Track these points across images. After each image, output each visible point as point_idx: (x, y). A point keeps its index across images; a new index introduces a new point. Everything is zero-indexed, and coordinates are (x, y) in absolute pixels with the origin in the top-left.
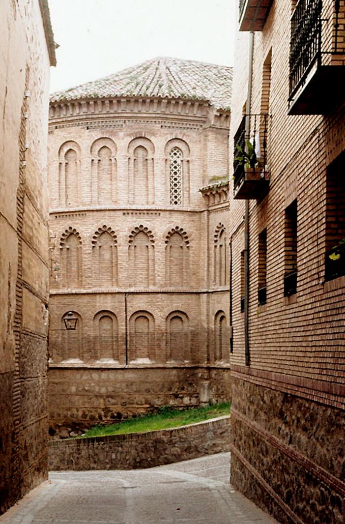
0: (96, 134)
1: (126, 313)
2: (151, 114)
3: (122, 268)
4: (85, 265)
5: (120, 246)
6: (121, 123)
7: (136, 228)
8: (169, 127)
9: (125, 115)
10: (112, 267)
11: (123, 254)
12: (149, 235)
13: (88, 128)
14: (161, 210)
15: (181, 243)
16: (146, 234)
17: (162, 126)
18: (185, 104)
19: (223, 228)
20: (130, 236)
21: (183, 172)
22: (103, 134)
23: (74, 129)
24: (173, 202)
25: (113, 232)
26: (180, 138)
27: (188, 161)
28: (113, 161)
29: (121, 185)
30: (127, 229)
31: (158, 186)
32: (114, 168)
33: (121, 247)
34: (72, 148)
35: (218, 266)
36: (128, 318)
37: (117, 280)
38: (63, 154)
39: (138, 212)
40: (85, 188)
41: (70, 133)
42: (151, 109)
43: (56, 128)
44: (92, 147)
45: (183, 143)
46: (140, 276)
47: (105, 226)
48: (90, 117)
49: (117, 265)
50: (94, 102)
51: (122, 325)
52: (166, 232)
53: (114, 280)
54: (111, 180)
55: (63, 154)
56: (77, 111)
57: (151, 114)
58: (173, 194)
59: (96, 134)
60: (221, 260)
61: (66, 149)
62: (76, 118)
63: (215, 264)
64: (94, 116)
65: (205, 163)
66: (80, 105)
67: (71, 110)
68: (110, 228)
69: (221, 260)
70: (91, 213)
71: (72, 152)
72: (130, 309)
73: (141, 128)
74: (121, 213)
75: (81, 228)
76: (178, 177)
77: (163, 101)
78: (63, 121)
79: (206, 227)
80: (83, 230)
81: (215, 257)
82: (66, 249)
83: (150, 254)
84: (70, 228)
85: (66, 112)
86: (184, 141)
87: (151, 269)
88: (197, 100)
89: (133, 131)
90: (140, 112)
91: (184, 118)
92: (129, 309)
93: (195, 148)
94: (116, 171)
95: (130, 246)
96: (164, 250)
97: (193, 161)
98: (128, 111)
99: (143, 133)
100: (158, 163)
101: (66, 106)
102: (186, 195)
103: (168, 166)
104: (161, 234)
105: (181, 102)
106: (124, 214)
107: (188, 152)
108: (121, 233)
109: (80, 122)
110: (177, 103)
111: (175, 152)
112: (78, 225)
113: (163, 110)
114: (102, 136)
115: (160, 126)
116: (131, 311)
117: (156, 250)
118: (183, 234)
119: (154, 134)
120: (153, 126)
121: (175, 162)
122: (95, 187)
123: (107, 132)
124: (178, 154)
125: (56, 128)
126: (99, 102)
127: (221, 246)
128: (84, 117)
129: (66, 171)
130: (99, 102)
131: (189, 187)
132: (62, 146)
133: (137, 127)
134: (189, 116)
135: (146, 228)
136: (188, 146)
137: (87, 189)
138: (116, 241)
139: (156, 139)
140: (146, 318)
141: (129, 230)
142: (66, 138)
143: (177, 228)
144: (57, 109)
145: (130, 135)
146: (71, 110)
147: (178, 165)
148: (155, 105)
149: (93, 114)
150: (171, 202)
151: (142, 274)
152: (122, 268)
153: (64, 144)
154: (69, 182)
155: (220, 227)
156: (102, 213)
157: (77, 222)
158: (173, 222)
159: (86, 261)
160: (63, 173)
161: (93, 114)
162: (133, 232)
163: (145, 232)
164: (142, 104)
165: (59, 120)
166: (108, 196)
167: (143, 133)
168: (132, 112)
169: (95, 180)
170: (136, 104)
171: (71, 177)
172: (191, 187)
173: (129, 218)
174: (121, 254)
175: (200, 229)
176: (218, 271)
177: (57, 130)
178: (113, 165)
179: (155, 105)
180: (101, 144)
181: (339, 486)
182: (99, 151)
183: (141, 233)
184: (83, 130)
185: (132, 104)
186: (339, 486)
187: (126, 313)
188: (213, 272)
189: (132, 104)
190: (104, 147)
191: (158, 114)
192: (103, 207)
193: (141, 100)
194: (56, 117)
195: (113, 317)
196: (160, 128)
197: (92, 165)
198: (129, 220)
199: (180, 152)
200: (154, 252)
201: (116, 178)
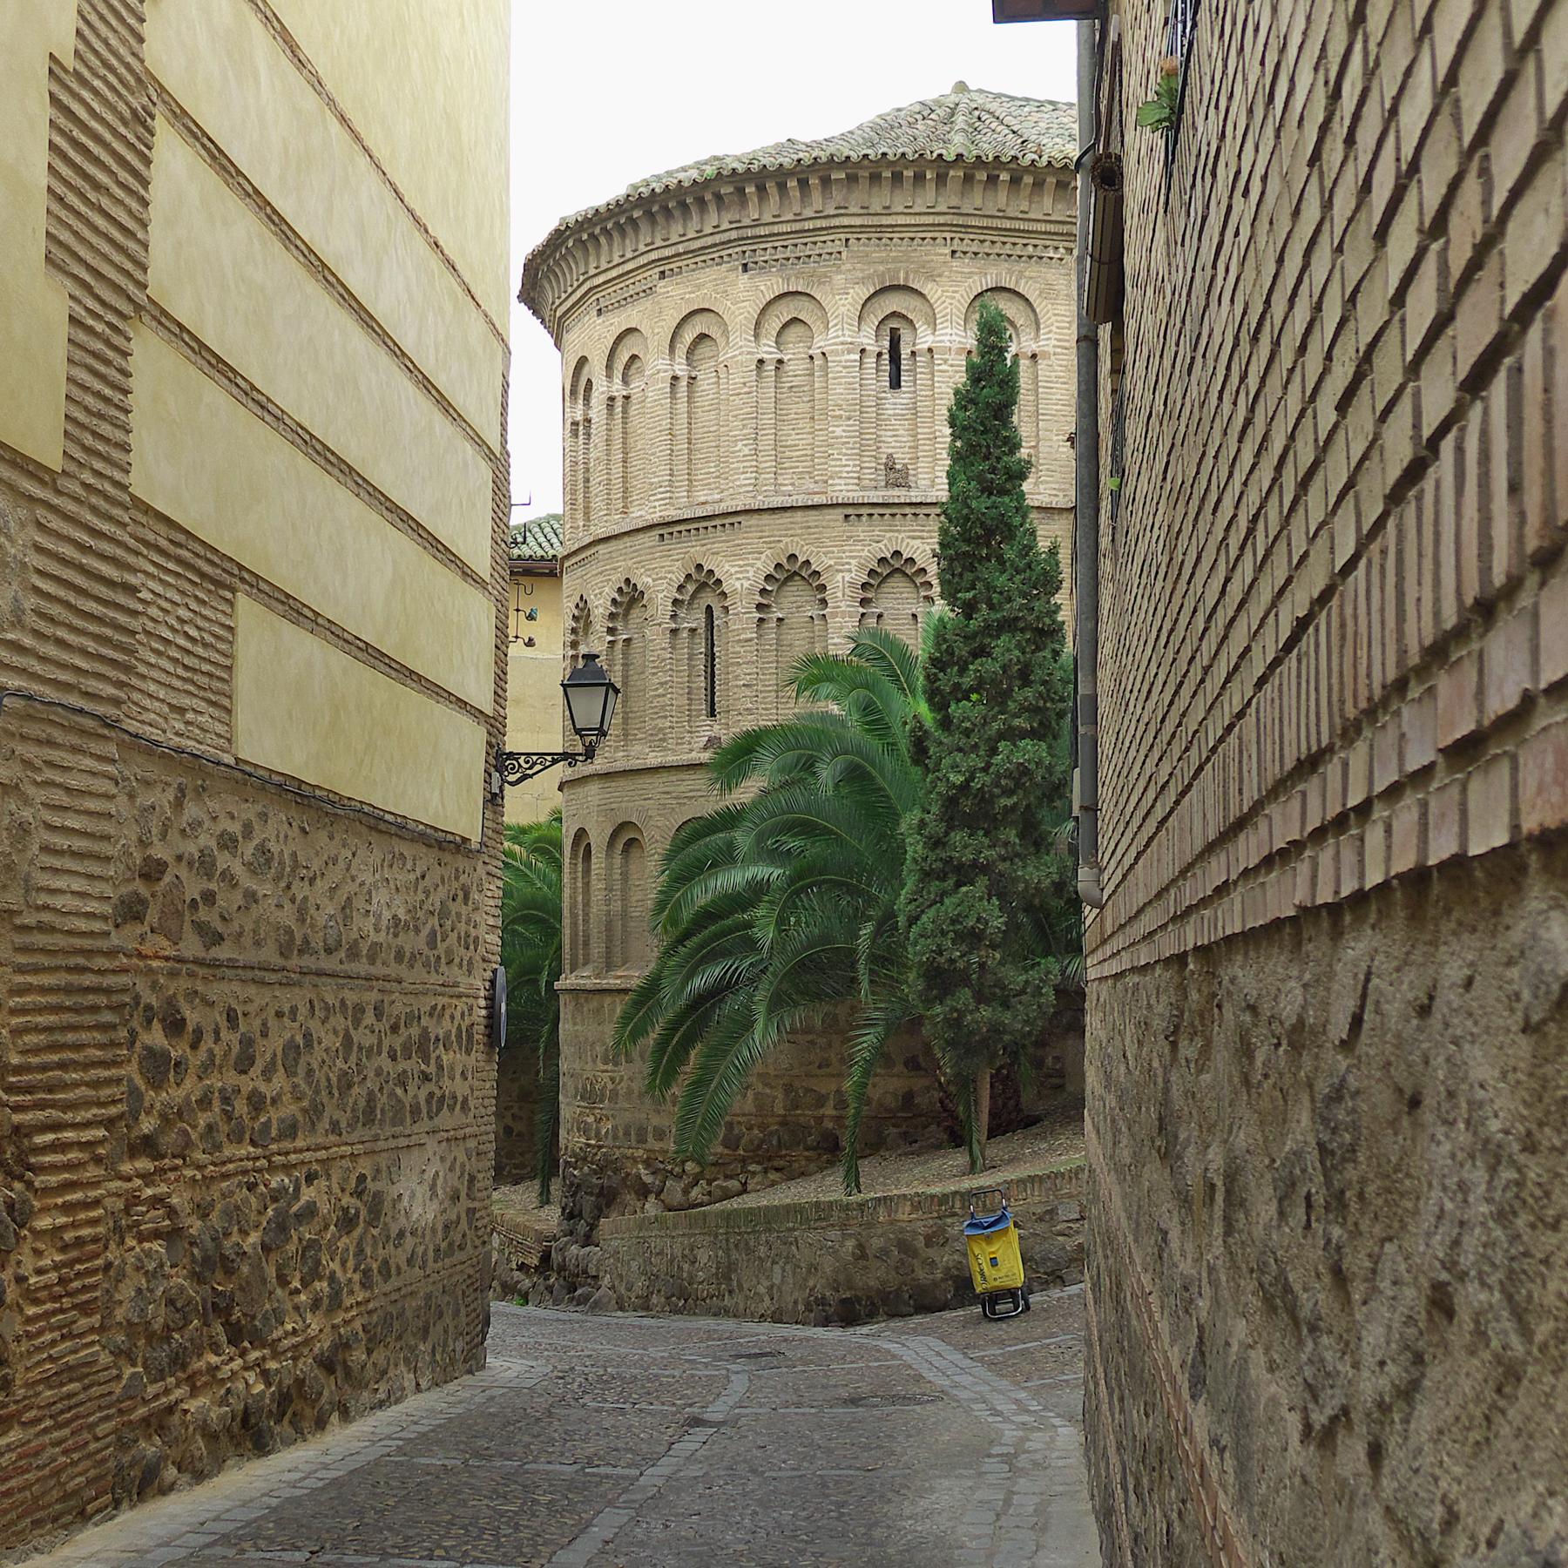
0: (772, 285)
5: (834, 615)
6: (838, 245)
7: (882, 561)
8: (976, 254)
9: (846, 221)
12: (919, 580)
13: (745, 267)
16: (911, 579)
17: (954, 252)
18: (1015, 181)
20: (864, 586)
23: (710, 274)
25: (816, 574)
29: (839, 432)
38: (681, 349)
39: (888, 511)
41: (699, 287)
42: (919, 201)
43: (662, 275)
44: (758, 324)
45: (915, 297)
47: (793, 557)
48: (750, 233)
50: (757, 187)
55: (681, 349)
56: (712, 218)
59: (772, 285)
61: (688, 336)
62: (709, 241)
64: (762, 231)
67: (695, 217)
70: (754, 520)
71: (708, 342)
73: (894, 260)
74: (838, 514)
77: (952, 173)
78: (679, 255)
82: (685, 634)
85: (685, 227)
88: (791, 173)
90: (887, 211)
97: (1046, 355)
98: (852, 210)
99: (902, 275)
101: (683, 206)
105: (1005, 176)
108: (839, 577)
109: (723, 253)
110: (992, 180)
113: (954, 201)
115: (947, 251)
118: (801, 567)
119: (931, 277)
122: (766, 442)
125: (662, 275)
126: (771, 186)
128: (734, 235)
130: (771, 186)
132: (679, 326)
134: (1029, 220)
135: (911, 560)
137: (743, 449)
138: (824, 602)
141: (861, 567)
144: (660, 219)
145: (862, 281)
146: (695, 217)
148: (931, 188)
149: (757, 224)
154: (698, 432)
156: (785, 518)
160: (682, 406)
161: (757, 224)
163: (910, 571)
164: (893, 186)
165: (667, 252)
167: (902, 275)
168: (866, 211)
169: (768, 419)
170: (875, 190)
171: (704, 418)
173: (861, 530)
177: (662, 283)
179: (931, 188)
180: (785, 312)
184: (732, 276)
185: (864, 184)
189: (864, 184)
190: (795, 320)
192: (788, 501)
193: (887, 174)
194: (659, 243)
196: (949, 258)
197: (758, 375)
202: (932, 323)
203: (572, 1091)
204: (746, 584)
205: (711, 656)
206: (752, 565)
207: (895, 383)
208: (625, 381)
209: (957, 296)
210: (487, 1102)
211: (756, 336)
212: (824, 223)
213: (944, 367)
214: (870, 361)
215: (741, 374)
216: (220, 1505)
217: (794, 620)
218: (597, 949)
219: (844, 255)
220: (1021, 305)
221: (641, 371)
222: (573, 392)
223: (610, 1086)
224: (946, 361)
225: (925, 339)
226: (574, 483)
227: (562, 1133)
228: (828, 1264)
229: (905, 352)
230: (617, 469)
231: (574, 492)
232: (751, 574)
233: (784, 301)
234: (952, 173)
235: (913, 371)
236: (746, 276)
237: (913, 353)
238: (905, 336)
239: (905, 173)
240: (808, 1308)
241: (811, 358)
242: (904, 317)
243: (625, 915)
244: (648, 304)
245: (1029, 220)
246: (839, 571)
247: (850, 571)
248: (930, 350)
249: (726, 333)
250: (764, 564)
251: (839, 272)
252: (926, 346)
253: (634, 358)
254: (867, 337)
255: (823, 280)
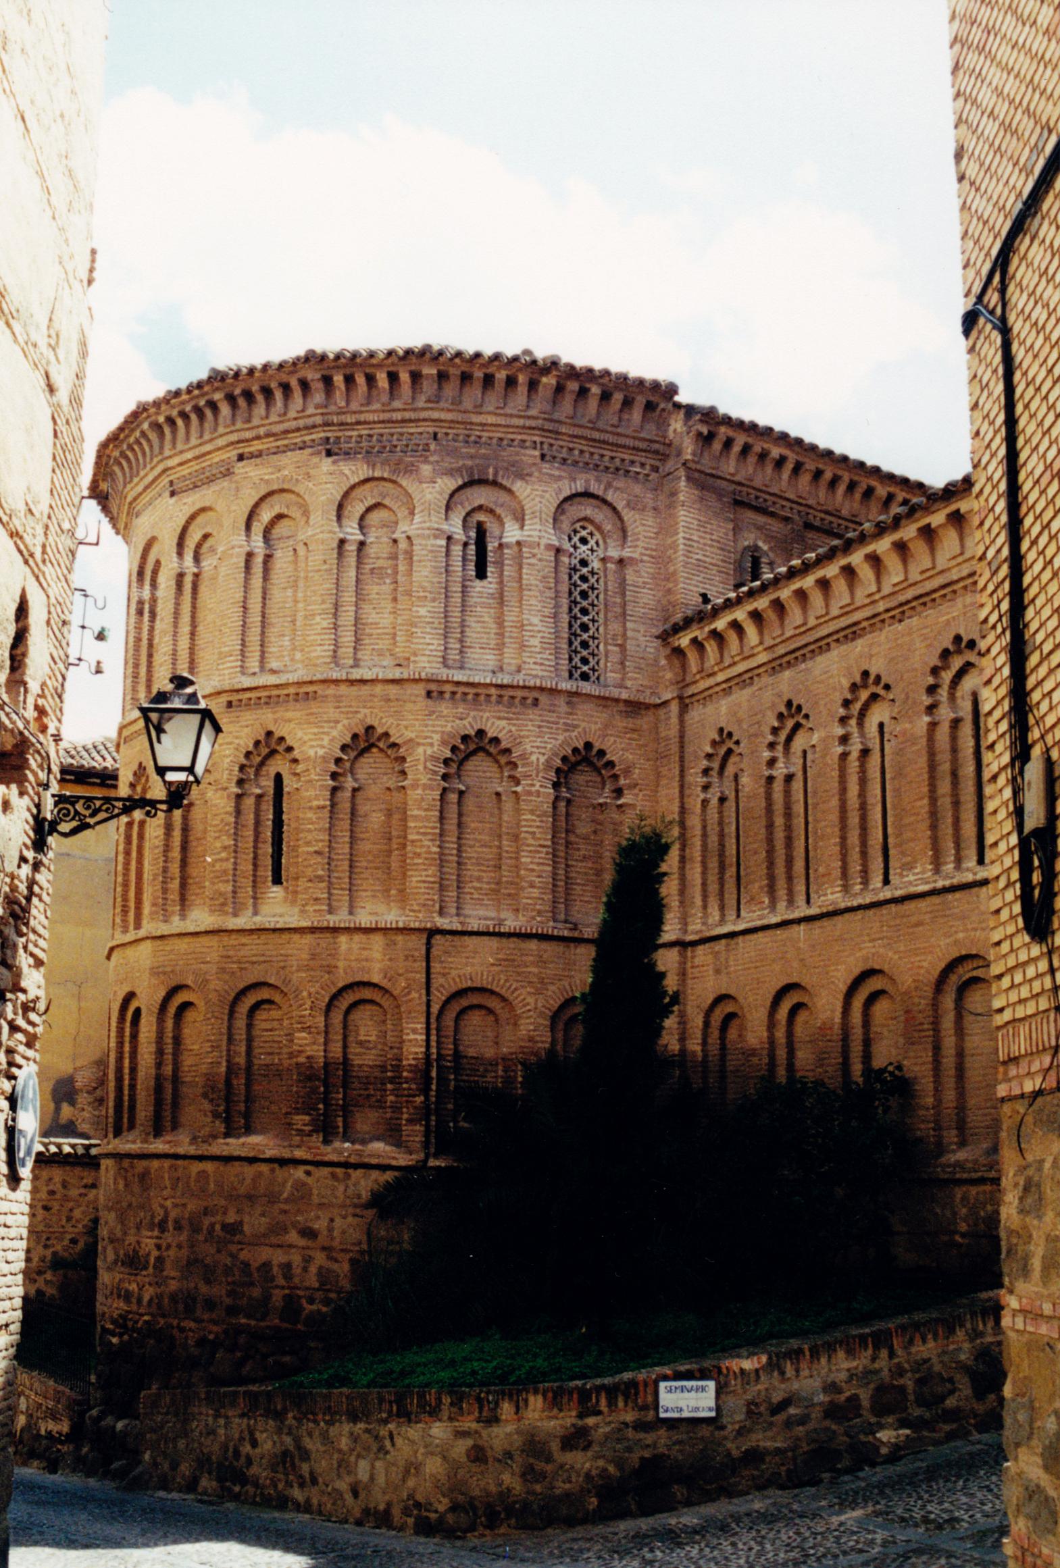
0: (355, 470)
1: (428, 993)
2: (511, 416)
3: (418, 855)
4: (308, 843)
7: (465, 738)
8: (565, 460)
10: (389, 852)
11: (423, 813)
14: (541, 689)
15: (600, 795)
19: (730, 744)
21: (606, 590)
22: (374, 466)
24: (577, 675)
25: (394, 745)
26: (600, 493)
27: (621, 561)
28: (403, 545)
29: (422, 611)
30: (436, 737)
31: (535, 620)
32: (402, 568)
33: (419, 791)
34: (285, 511)
35: (713, 864)
36: (435, 1009)
37: (401, 891)
40: (318, 619)
43: (241, 458)
44: (340, 507)
46: (476, 884)
47: (370, 729)
49: (404, 846)
51: (414, 1031)
52: (556, 755)
53: (393, 892)
54: (395, 600)
55: (258, 528)
57: (511, 416)
58: (576, 652)
60: (722, 845)
61: (266, 516)
63: (704, 857)
65: (672, 569)
66: (305, 385)
68: (386, 735)
69: (722, 845)
71: (285, 522)
72: (441, 980)
74: (420, 690)
75: (300, 734)
76: (593, 638)
79: (675, 748)
80: (306, 738)
81: (705, 835)
83: (505, 818)
84: (269, 734)
86: (610, 505)
87: (507, 863)
89: (461, 463)
91: (606, 437)
92: (437, 981)
93: (641, 525)
94: (410, 572)
95: (445, 790)
96: (547, 807)
99: (491, 470)
100: (534, 556)
102: (615, 657)
103: (564, 571)
104: (542, 759)
106: (429, 694)
107: (620, 534)
111: (584, 533)
112: (292, 725)
114: (370, 474)
115: (537, 453)
116: (443, 987)
117: (523, 806)
119: (522, 476)
120: (517, 454)
121: (584, 563)
122: (347, 618)
123: (385, 463)
124: (592, 543)
127: (722, 800)
129: (266, 578)
131: (624, 634)
133: (473, 451)
134: (619, 434)
135: (496, 740)
136: (620, 519)
138: (403, 773)
139: (529, 487)
140: (490, 1011)
141: (444, 743)
142: (267, 482)
143: (588, 745)
145: (450, 473)
147: (592, 573)
150: (571, 676)
151: (479, 879)
152: (418, 855)
153: (263, 499)
155: (723, 742)
157: (290, 715)
158: (576, 726)
159: (309, 831)
162: (454, 749)
166: (383, 644)
167: (491, 470)
172: (629, 634)
174: (416, 812)
175: (660, 757)
176: (713, 878)
177: (240, 464)
178: (401, 557)
180: (368, 496)
181: (418, 1393)
182: (362, 518)
183: (481, 754)
184: (315, 460)
186: (418, 1393)
187: (428, 993)
188: (698, 881)
191: (529, 417)
195: (386, 1002)
196: (538, 460)
198: (445, 712)
199: (598, 536)
200: (518, 811)
201: (409, 593)
202: (520, 519)
203: (111, 1256)
204: (321, 752)
205: (278, 823)
206: (327, 734)
207: (481, 574)
208: (197, 558)
209: (547, 495)
210: (11, 1256)
211: (339, 517)
212: (412, 415)
213: (533, 561)
214: (457, 550)
215: (320, 554)
216: (246, 1000)
217: (374, 790)
218: (144, 1112)
219: (432, 447)
220: (607, 511)
221: (213, 550)
222: (141, 573)
223: (155, 1253)
224: (534, 556)
225: (512, 534)
226: (138, 640)
227: (100, 1298)
228: (434, 1466)
229: (491, 546)
230: (184, 643)
231: (136, 666)
232: (326, 742)
233: (368, 486)
234: (544, 380)
235: (500, 564)
236: (330, 460)
237: (501, 546)
238: (492, 527)
239: (498, 376)
240: (406, 1512)
241: (395, 541)
242: (492, 511)
243: (176, 1078)
244: (225, 484)
245: (619, 434)
246: (419, 744)
247: (431, 745)
248: (519, 543)
249: (306, 513)
250: (340, 733)
251: (426, 461)
252: (514, 540)
253: (206, 536)
254: (455, 526)
255: (410, 470)
